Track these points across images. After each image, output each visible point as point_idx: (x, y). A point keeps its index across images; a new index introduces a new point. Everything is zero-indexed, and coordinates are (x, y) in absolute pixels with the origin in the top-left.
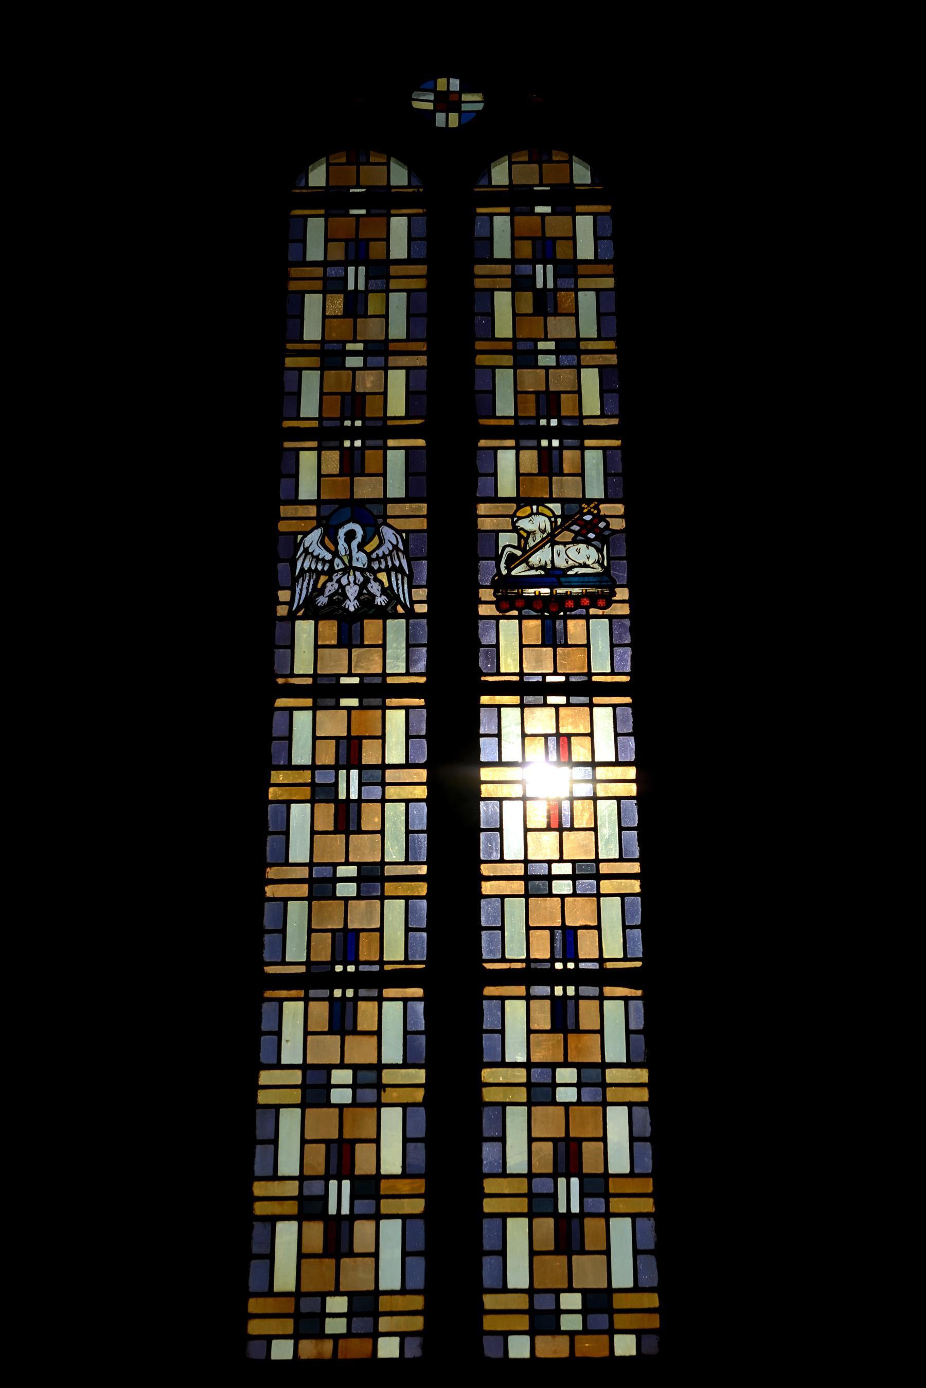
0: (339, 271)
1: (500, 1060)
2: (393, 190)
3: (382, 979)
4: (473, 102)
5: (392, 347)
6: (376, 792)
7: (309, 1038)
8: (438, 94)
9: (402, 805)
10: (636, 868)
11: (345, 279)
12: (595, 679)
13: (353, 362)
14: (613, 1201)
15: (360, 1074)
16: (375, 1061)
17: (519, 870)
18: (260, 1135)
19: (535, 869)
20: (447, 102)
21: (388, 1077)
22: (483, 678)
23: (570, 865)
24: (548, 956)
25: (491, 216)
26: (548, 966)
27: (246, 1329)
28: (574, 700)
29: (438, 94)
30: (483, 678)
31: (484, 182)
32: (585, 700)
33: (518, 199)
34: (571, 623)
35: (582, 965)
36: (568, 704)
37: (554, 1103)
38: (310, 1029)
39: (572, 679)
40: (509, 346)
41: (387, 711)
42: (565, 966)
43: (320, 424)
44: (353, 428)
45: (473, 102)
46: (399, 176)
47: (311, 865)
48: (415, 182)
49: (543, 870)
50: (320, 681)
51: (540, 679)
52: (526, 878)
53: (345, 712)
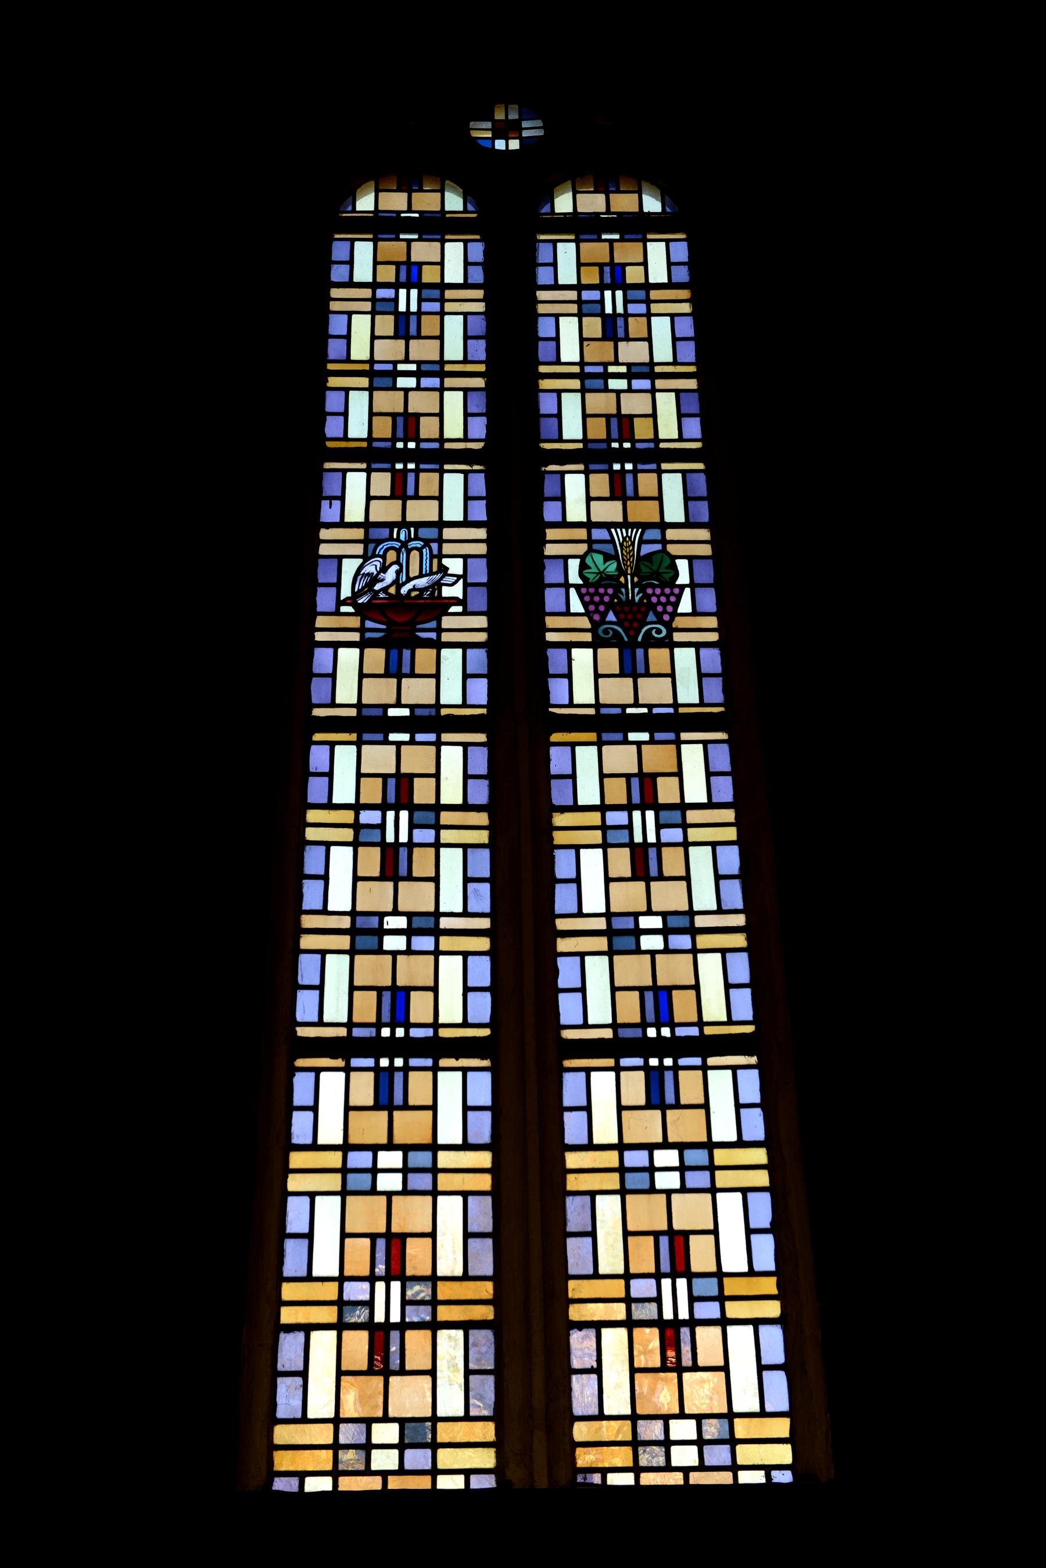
0: (389, 293)
1: (571, 803)
2: (448, 216)
3: (438, 1049)
4: (532, 129)
5: (448, 368)
6: (428, 836)
7: (347, 1241)
8: (495, 122)
9: (459, 959)
10: (740, 920)
11: (396, 300)
12: (662, 445)
13: (392, 943)
14: (718, 1174)
15: (412, 1155)
16: (433, 801)
17: (601, 924)
18: (309, 869)
19: (618, 924)
20: (503, 130)
21: (445, 1433)
22: (551, 710)
23: (659, 919)
24: (604, 436)
25: (562, 474)
26: (604, 446)
27: (305, 817)
28: (658, 736)
29: (495, 122)
30: (551, 710)
31: (546, 209)
32: (671, 736)
33: (581, 226)
34: (653, 652)
35: (638, 445)
36: (652, 741)
37: (606, 390)
38: (360, 874)
39: (655, 711)
40: (576, 369)
41: (442, 802)
42: (661, 1062)
43: (359, 712)
44: (401, 625)
45: (532, 129)
46: (454, 202)
47: (353, 913)
48: (470, 208)
49: (628, 923)
50: (366, 712)
51: (618, 711)
52: (609, 933)
53: (384, 1198)
